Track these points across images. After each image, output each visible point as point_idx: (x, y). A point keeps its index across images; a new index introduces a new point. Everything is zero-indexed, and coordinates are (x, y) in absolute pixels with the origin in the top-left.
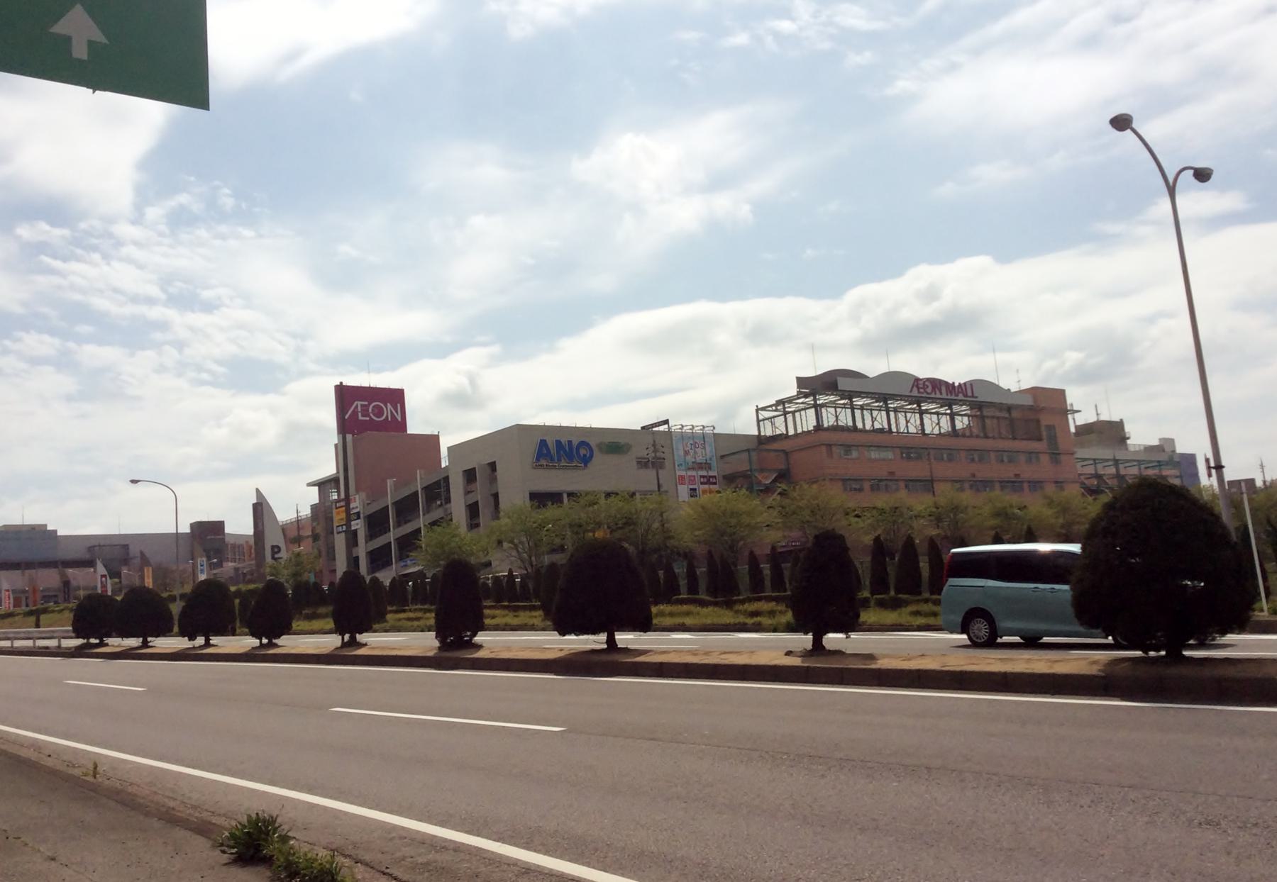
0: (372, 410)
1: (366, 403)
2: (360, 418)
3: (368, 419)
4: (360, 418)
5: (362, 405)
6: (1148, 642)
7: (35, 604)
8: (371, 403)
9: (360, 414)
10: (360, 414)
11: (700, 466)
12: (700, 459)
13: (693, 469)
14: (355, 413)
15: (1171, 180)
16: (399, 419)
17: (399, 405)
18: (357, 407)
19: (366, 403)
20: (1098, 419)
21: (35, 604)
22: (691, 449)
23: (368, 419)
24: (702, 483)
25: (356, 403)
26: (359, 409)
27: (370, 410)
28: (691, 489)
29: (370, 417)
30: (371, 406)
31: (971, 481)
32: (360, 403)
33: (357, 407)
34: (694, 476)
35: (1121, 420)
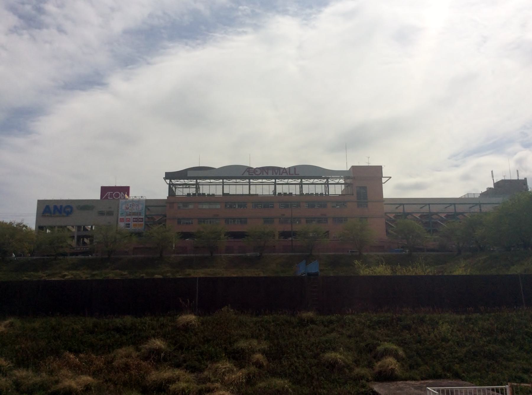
0: (115, 195)
1: (112, 192)
5: (110, 193)
6: (399, 264)
7: (276, 174)
8: (114, 192)
10: (109, 197)
11: (134, 214)
12: (135, 211)
13: (130, 215)
15: (389, 178)
18: (108, 194)
19: (112, 192)
20: (518, 179)
21: (276, 174)
22: (130, 207)
24: (133, 221)
26: (109, 195)
27: (114, 195)
28: (129, 227)
29: (113, 198)
30: (114, 194)
31: (118, 211)
32: (109, 193)
33: (108, 194)
34: (130, 218)
35: (526, 179)
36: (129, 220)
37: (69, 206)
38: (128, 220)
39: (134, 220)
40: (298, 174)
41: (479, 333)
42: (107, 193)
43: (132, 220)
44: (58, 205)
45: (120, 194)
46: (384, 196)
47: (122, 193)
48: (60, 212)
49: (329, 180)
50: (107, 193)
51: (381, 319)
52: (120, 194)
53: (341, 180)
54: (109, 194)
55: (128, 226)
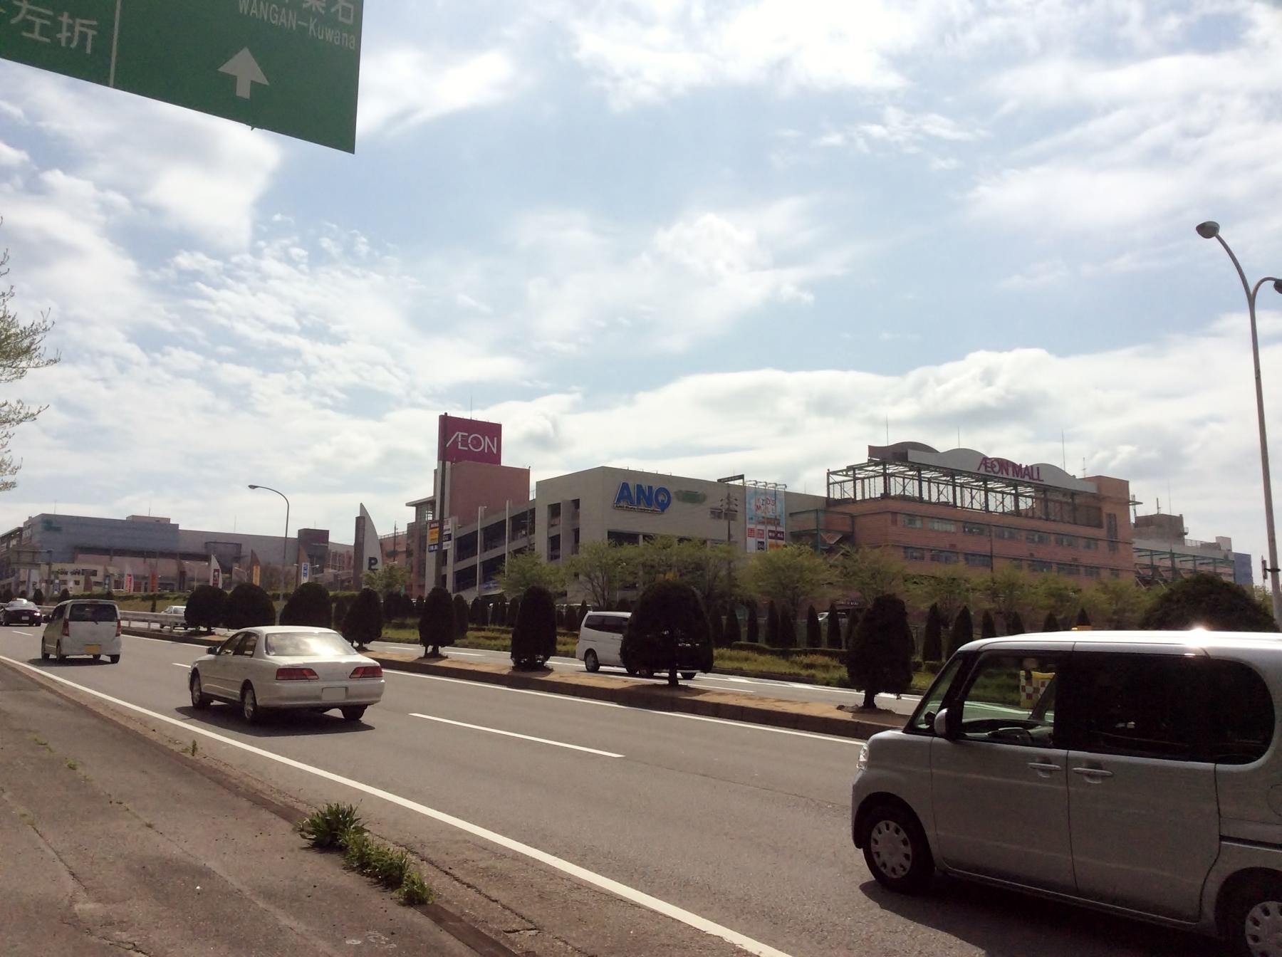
0: (471, 441)
1: (467, 434)
2: (460, 447)
3: (466, 449)
4: (460, 447)
8: (471, 434)
9: (460, 444)
10: (460, 444)
12: (770, 514)
14: (455, 442)
16: (495, 452)
17: (495, 439)
18: (458, 435)
19: (467, 434)
23: (466, 449)
24: (770, 538)
25: (457, 433)
27: (469, 441)
29: (468, 447)
32: (460, 434)
33: (458, 435)
35: (1181, 515)
36: (761, 533)
37: (663, 490)
38: (761, 534)
39: (770, 534)
40: (1042, 481)
41: (619, 945)
42: (456, 435)
43: (766, 534)
44: (645, 485)
45: (482, 439)
46: (713, 480)
47: (487, 438)
48: (649, 504)
49: (882, 471)
50: (456, 435)
51: (120, 933)
52: (482, 439)
53: (1029, 489)
54: (460, 436)
55: (761, 546)
